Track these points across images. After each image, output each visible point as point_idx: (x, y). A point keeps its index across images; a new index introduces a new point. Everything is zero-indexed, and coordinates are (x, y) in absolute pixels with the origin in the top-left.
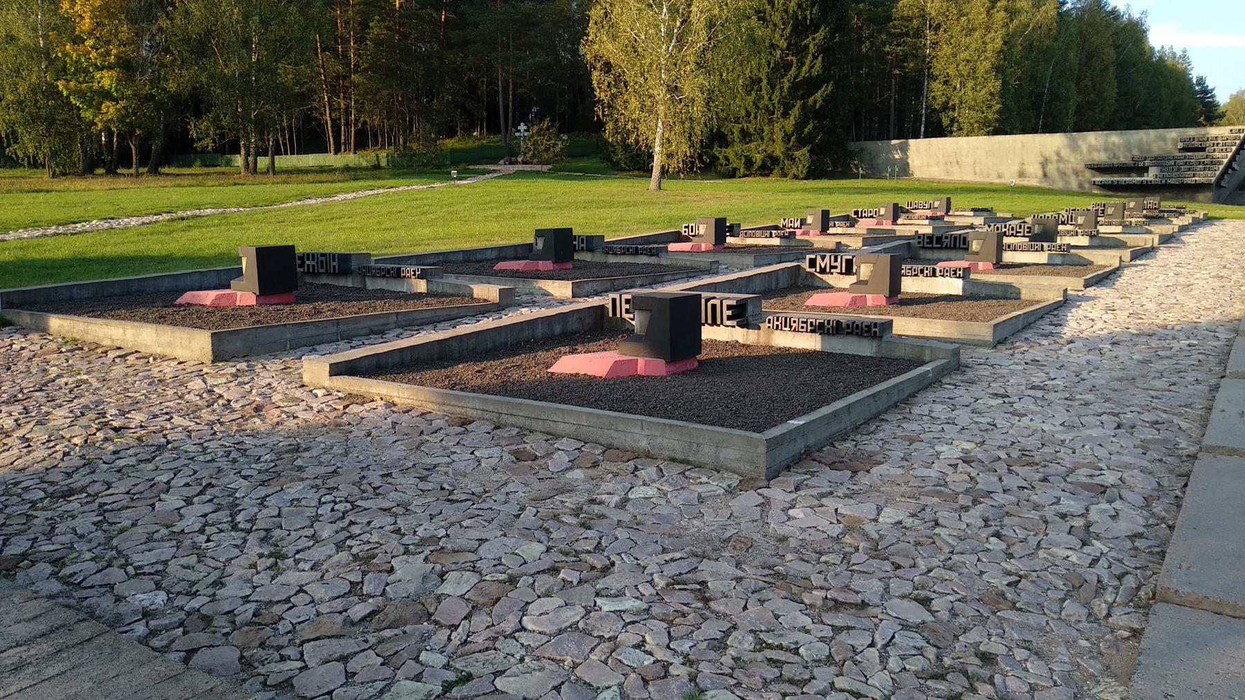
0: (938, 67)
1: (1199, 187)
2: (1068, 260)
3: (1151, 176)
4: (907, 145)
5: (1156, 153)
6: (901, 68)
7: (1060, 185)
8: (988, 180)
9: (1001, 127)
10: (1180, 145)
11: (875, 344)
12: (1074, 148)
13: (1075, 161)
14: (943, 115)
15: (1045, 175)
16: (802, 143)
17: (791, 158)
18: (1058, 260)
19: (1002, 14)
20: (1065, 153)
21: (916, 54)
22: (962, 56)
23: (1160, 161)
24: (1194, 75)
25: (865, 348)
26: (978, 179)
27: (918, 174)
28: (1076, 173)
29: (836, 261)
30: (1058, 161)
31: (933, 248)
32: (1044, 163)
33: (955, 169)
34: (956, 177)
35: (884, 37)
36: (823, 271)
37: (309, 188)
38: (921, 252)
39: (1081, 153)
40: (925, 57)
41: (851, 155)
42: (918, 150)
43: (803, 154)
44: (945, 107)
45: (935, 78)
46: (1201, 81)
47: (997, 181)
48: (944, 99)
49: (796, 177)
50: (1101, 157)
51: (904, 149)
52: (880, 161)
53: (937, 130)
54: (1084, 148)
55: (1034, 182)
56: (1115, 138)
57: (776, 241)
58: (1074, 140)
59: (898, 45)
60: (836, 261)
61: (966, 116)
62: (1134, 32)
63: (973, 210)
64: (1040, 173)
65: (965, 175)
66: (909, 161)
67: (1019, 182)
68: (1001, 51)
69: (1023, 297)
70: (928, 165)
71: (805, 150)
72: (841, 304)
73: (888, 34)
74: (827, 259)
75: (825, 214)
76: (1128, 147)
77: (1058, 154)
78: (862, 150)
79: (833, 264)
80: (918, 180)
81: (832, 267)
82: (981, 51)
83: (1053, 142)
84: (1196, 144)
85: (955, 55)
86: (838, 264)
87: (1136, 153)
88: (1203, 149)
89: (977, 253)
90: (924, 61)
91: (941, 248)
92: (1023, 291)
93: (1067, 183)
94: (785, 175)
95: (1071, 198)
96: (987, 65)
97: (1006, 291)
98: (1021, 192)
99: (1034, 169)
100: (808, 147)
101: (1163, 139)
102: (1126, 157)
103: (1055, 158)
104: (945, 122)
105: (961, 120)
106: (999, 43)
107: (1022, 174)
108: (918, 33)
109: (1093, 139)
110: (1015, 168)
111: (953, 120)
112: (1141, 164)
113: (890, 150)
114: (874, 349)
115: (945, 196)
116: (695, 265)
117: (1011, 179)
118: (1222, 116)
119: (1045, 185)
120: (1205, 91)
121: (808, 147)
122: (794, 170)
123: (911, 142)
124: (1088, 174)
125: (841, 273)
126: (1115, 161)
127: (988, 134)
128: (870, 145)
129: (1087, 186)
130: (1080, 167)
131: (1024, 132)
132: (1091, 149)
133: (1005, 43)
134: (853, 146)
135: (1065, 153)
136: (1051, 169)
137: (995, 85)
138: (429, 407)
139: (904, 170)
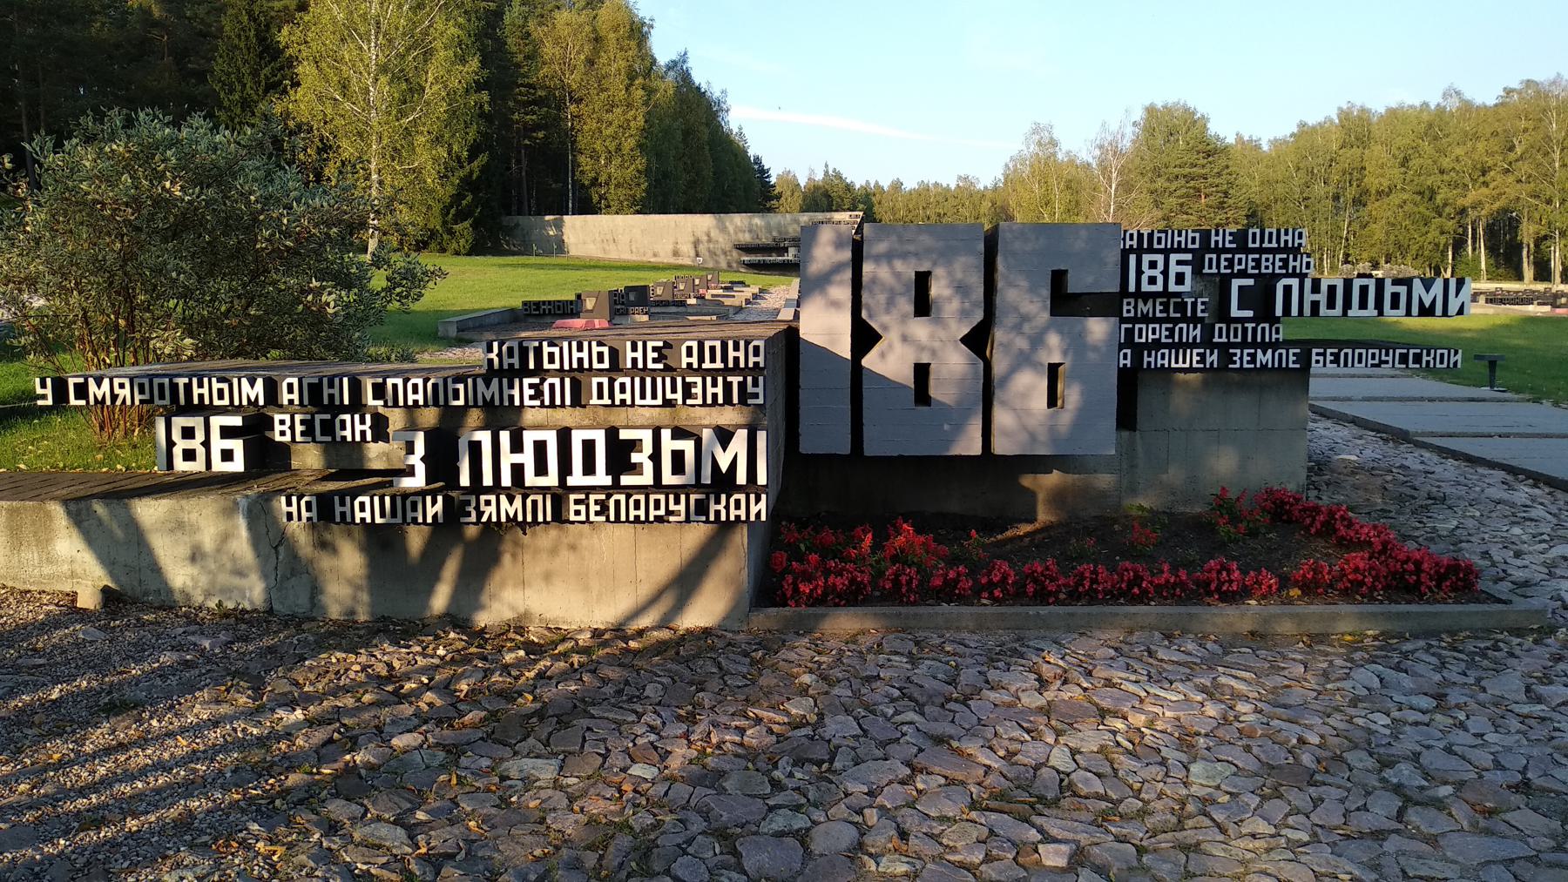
0: (582, 141)
6: (530, 138)
12: (723, 229)
13: (723, 242)
14: (593, 190)
16: (461, 216)
17: (451, 232)
19: (641, 92)
20: (714, 234)
21: (553, 123)
22: (609, 131)
24: (751, 153)
26: (634, 258)
27: (573, 252)
28: (725, 253)
32: (696, 243)
33: (612, 247)
34: (613, 255)
35: (511, 104)
37: (671, 322)
41: (510, 231)
42: (573, 227)
43: (464, 227)
44: (595, 182)
46: (758, 160)
48: (593, 174)
49: (457, 253)
50: (746, 238)
51: (559, 226)
53: (586, 207)
55: (688, 262)
61: (614, 194)
62: (1204, 120)
64: (692, 253)
67: (673, 261)
71: (467, 224)
73: (516, 101)
76: (769, 228)
78: (517, 225)
80: (573, 257)
82: (625, 127)
83: (703, 223)
94: (443, 250)
96: (632, 142)
99: (687, 248)
100: (470, 221)
104: (595, 198)
106: (641, 121)
107: (676, 253)
108: (561, 105)
109: (738, 220)
110: (670, 247)
111: (601, 197)
117: (666, 258)
120: (763, 172)
121: (470, 221)
122: (454, 245)
124: (735, 253)
127: (638, 212)
128: (523, 220)
130: (728, 247)
131: (677, 212)
132: (738, 230)
134: (506, 220)
136: (702, 248)
137: (641, 163)
139: (560, 246)
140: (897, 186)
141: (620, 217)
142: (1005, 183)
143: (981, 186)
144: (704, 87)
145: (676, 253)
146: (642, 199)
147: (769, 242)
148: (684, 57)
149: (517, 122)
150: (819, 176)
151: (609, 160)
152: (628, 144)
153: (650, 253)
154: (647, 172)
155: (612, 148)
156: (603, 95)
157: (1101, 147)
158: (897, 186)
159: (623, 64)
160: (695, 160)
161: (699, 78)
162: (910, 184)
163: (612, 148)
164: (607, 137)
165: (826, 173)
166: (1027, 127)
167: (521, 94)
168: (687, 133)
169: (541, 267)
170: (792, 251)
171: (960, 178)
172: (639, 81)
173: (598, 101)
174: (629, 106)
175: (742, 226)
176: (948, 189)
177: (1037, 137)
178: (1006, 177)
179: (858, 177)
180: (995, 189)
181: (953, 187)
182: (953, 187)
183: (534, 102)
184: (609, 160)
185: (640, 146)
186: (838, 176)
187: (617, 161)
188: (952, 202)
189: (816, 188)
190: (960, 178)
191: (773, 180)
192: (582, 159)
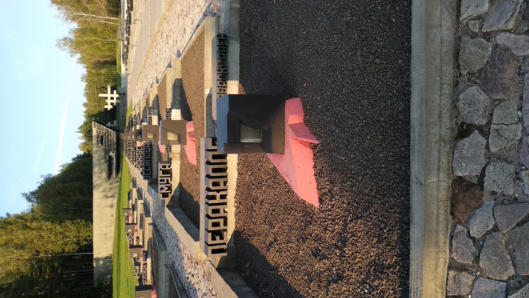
1: (118, 138)
2: (156, 106)
3: (113, 154)
4: (96, 258)
5: (103, 154)
7: (117, 190)
8: (114, 220)
9: (89, 219)
10: (100, 145)
11: (231, 41)
12: (100, 185)
13: (106, 185)
15: (112, 196)
18: (156, 111)
19: (34, 224)
20: (101, 189)
21: (50, 261)
22: (53, 238)
23: (107, 152)
25: (235, 49)
26: (114, 225)
28: (111, 184)
29: (163, 180)
30: (106, 192)
31: (151, 171)
33: (108, 235)
35: (40, 279)
36: (170, 188)
38: (154, 178)
39: (102, 183)
40: (53, 256)
41: (100, 284)
42: (99, 253)
45: (63, 250)
46: (74, 159)
47: (115, 217)
50: (104, 175)
51: (98, 260)
52: (104, 271)
53: (90, 247)
54: (100, 181)
55: (115, 201)
56: (96, 169)
57: (149, 261)
58: (96, 186)
59: (46, 272)
60: (163, 180)
61: (83, 234)
63: (129, 200)
65: (112, 231)
66: (104, 257)
67: (115, 207)
68: (52, 222)
69: (180, 77)
70: (107, 248)
72: (194, 145)
73: (39, 277)
74: (163, 186)
75: (132, 246)
76: (100, 165)
77: (103, 192)
78: (98, 280)
79: (166, 182)
80: (114, 251)
81: (168, 183)
83: (97, 195)
84: (100, 139)
85: (53, 242)
86: (165, 179)
87: (103, 161)
88: (102, 136)
89: (154, 135)
90: (54, 257)
91: (151, 166)
92: (177, 77)
93: (115, 187)
95: (121, 236)
97: (177, 86)
98: (120, 204)
99: (109, 201)
101: (97, 151)
102: (104, 165)
103: (104, 193)
105: (85, 236)
106: (48, 223)
107: (112, 206)
108: (41, 260)
109: (95, 179)
110: (109, 209)
111: (85, 240)
112: (108, 159)
113: (98, 267)
114: (235, 42)
115: (121, 210)
116: (168, 279)
117: (114, 211)
118: (89, 151)
119: (117, 196)
120: (78, 157)
123: (94, 257)
124: (111, 180)
125: (171, 177)
126: (106, 169)
128: (96, 276)
129: (117, 180)
133: (48, 220)
134: (96, 284)
135: (101, 189)
136: (109, 194)
137: (68, 223)
138: (444, 259)
139: (108, 259)
140: (85, 105)
141: (94, 232)
142: (85, 63)
143: (86, 73)
144: (39, 185)
145: (112, 206)
146: (86, 221)
147: (106, 164)
148: (24, 195)
149: (49, 276)
150: (81, 135)
151: (68, 237)
152: (59, 228)
153: (112, 218)
154: (72, 219)
155: (61, 236)
156: (35, 241)
157: (67, 19)
158: (85, 105)
159: (19, 232)
160: (67, 195)
161: (34, 187)
162: (85, 100)
163: (61, 236)
164: (56, 239)
165: (80, 132)
166: (58, 50)
167: (36, 275)
168: (59, 193)
169: (119, 270)
170: (111, 154)
171: (82, 81)
172: (28, 224)
173: (38, 243)
174: (41, 229)
175: (99, 176)
176: (87, 85)
177: (62, 45)
178: (82, 63)
179: (82, 120)
180: (87, 67)
181: (86, 83)
182: (86, 83)
183: (41, 270)
184: (68, 237)
185: (60, 223)
186: (81, 127)
187: (67, 234)
188: (92, 84)
189: (85, 136)
190: (82, 81)
191: (82, 153)
192: (66, 250)
